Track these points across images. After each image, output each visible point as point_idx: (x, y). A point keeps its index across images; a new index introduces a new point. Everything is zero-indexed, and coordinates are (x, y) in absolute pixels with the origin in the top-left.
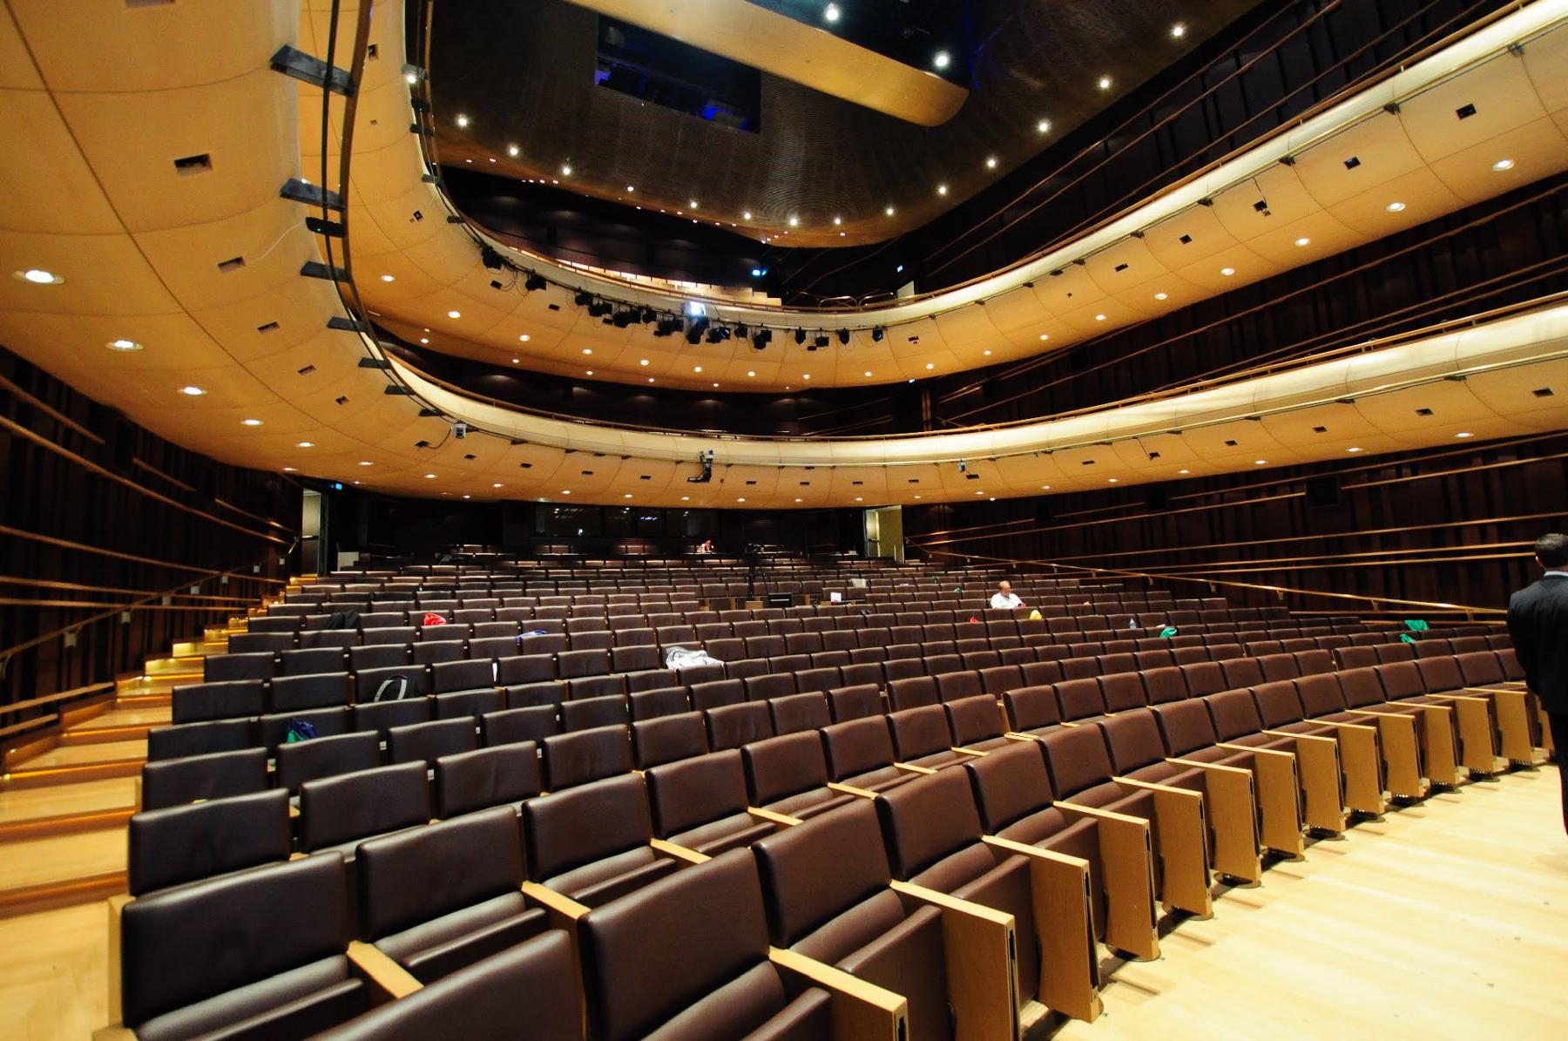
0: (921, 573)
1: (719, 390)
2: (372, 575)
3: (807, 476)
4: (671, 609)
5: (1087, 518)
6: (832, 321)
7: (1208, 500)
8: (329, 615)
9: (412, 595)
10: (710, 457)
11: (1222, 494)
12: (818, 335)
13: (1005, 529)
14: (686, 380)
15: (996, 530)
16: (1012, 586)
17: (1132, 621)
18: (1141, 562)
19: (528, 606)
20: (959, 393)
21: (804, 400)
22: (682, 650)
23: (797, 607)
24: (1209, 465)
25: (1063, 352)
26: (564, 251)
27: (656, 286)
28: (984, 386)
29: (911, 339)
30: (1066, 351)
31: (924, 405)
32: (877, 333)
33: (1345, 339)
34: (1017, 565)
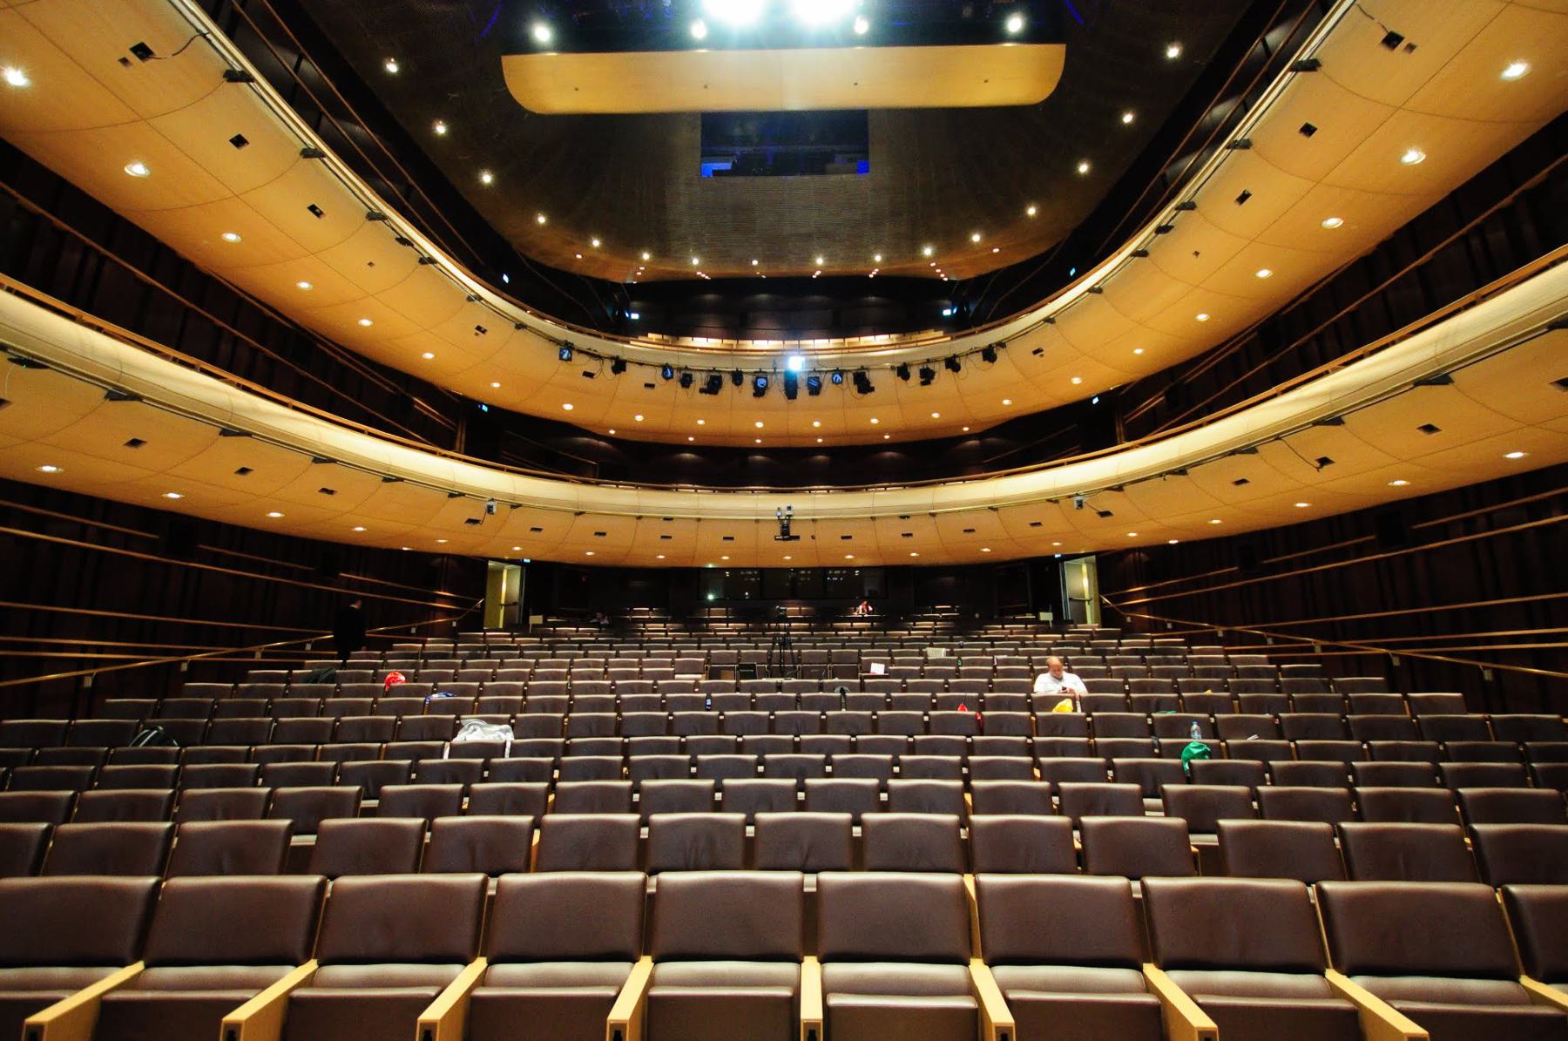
0: (696, 639)
1: (891, 442)
2: (583, 631)
3: (906, 526)
4: (641, 675)
5: (1305, 562)
6: (581, 340)
7: (1470, 526)
8: (310, 671)
9: (1047, 651)
10: (789, 513)
11: (1489, 515)
12: (921, 367)
13: (1207, 582)
14: (860, 433)
15: (1197, 584)
16: (1065, 661)
17: (1195, 726)
18: (1379, 629)
19: (918, 666)
20: (1143, 408)
21: (991, 440)
22: (483, 723)
23: (764, 680)
24: (1424, 469)
25: (1250, 334)
26: (705, 329)
27: (713, 346)
28: (1167, 394)
29: (1036, 352)
30: (1254, 331)
31: (1118, 430)
32: (989, 354)
33: (1159, 203)
34: (1224, 632)
